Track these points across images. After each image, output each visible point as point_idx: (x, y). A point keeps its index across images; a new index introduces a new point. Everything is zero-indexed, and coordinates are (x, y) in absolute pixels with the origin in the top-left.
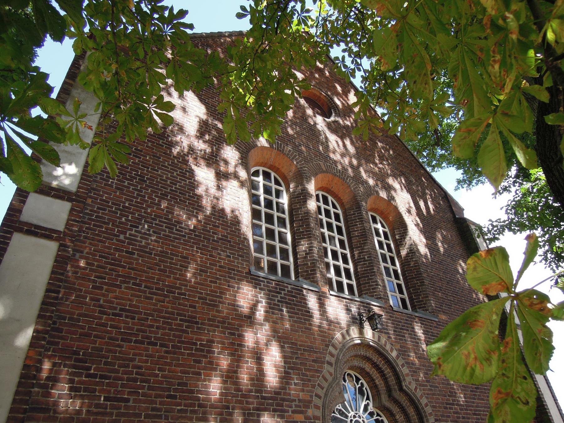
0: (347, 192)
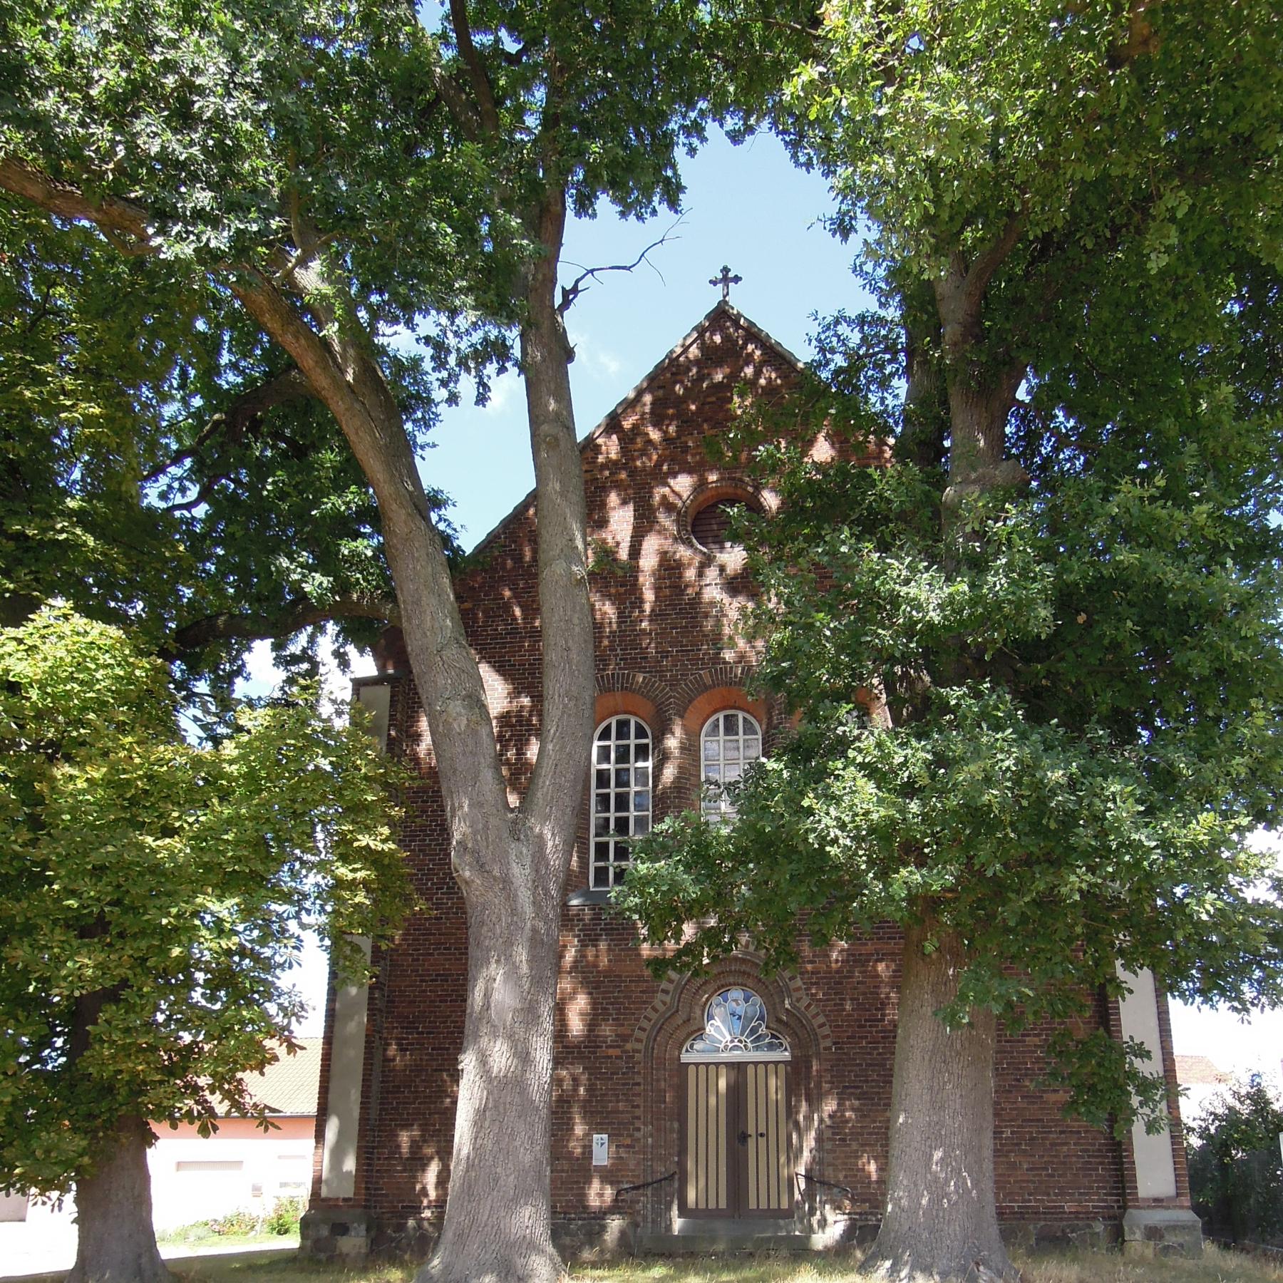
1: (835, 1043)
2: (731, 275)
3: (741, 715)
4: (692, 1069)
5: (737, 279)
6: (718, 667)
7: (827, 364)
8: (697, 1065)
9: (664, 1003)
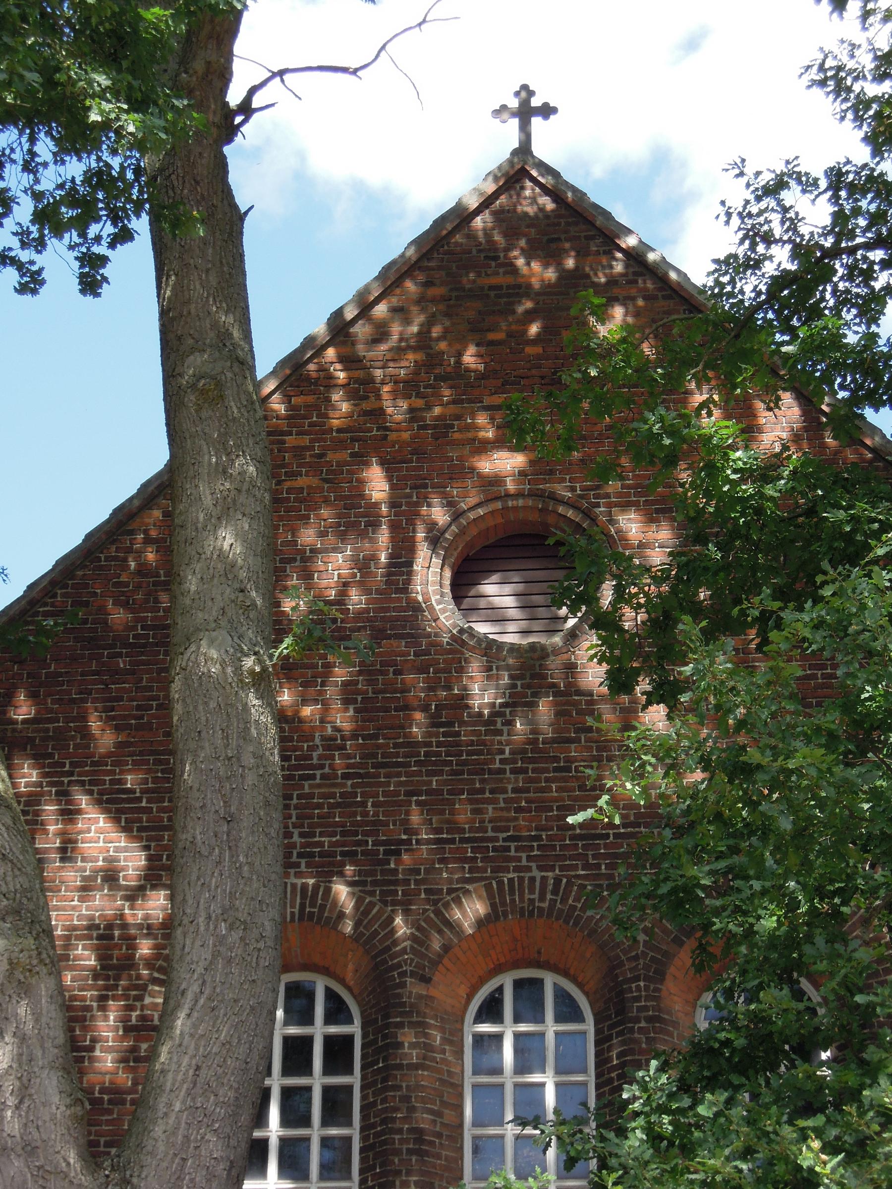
0: (588, 955)
2: (536, 102)
3: (550, 980)
5: (547, 111)
6: (506, 877)
7: (757, 264)
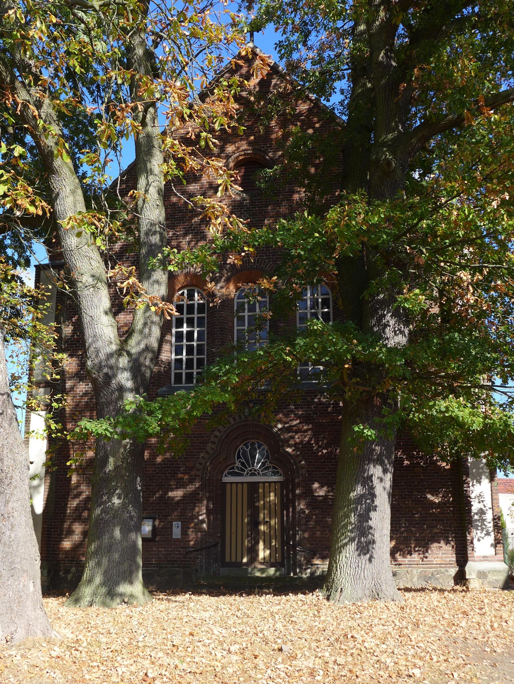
1: (307, 471)
4: (228, 486)
8: (231, 483)
9: (213, 449)
